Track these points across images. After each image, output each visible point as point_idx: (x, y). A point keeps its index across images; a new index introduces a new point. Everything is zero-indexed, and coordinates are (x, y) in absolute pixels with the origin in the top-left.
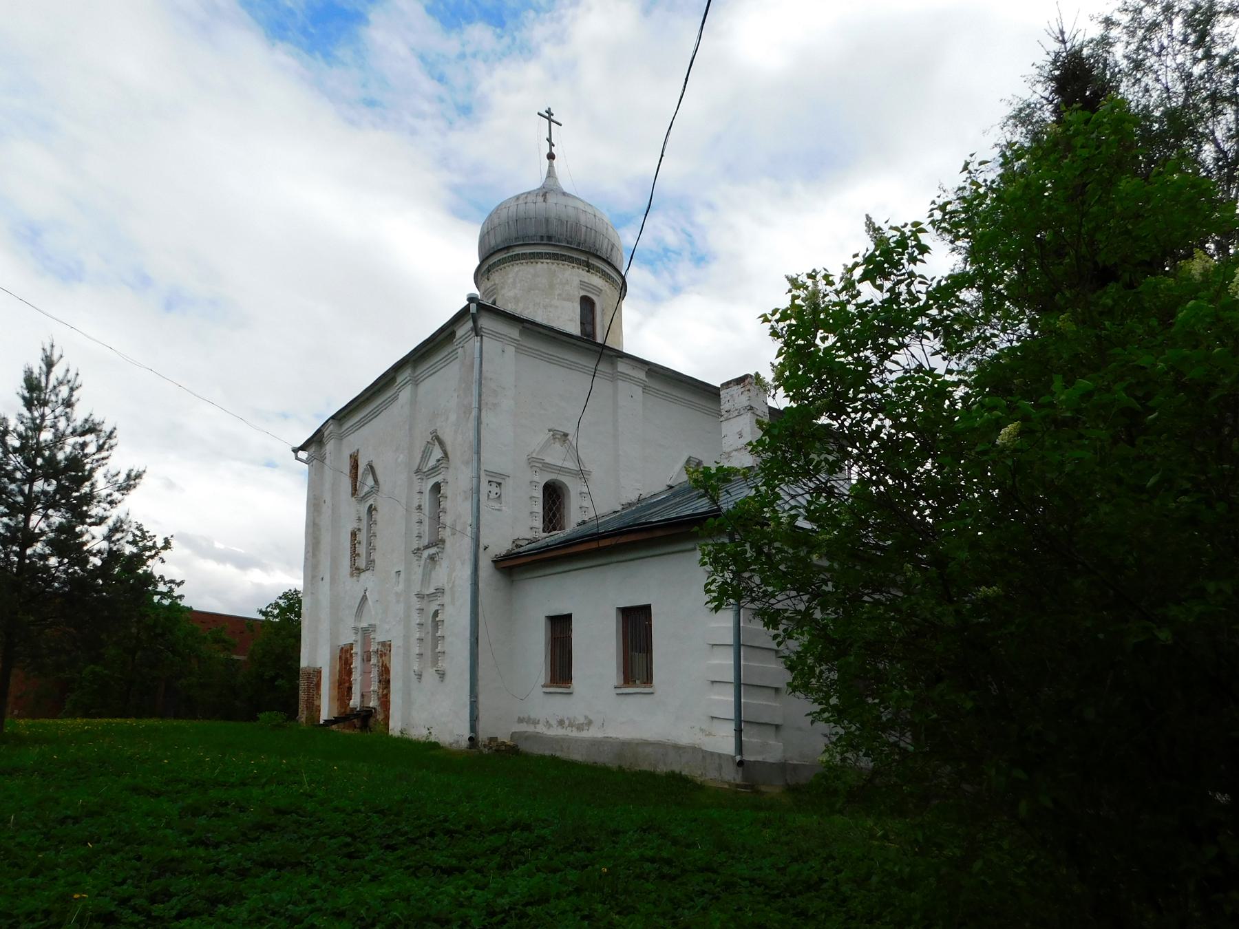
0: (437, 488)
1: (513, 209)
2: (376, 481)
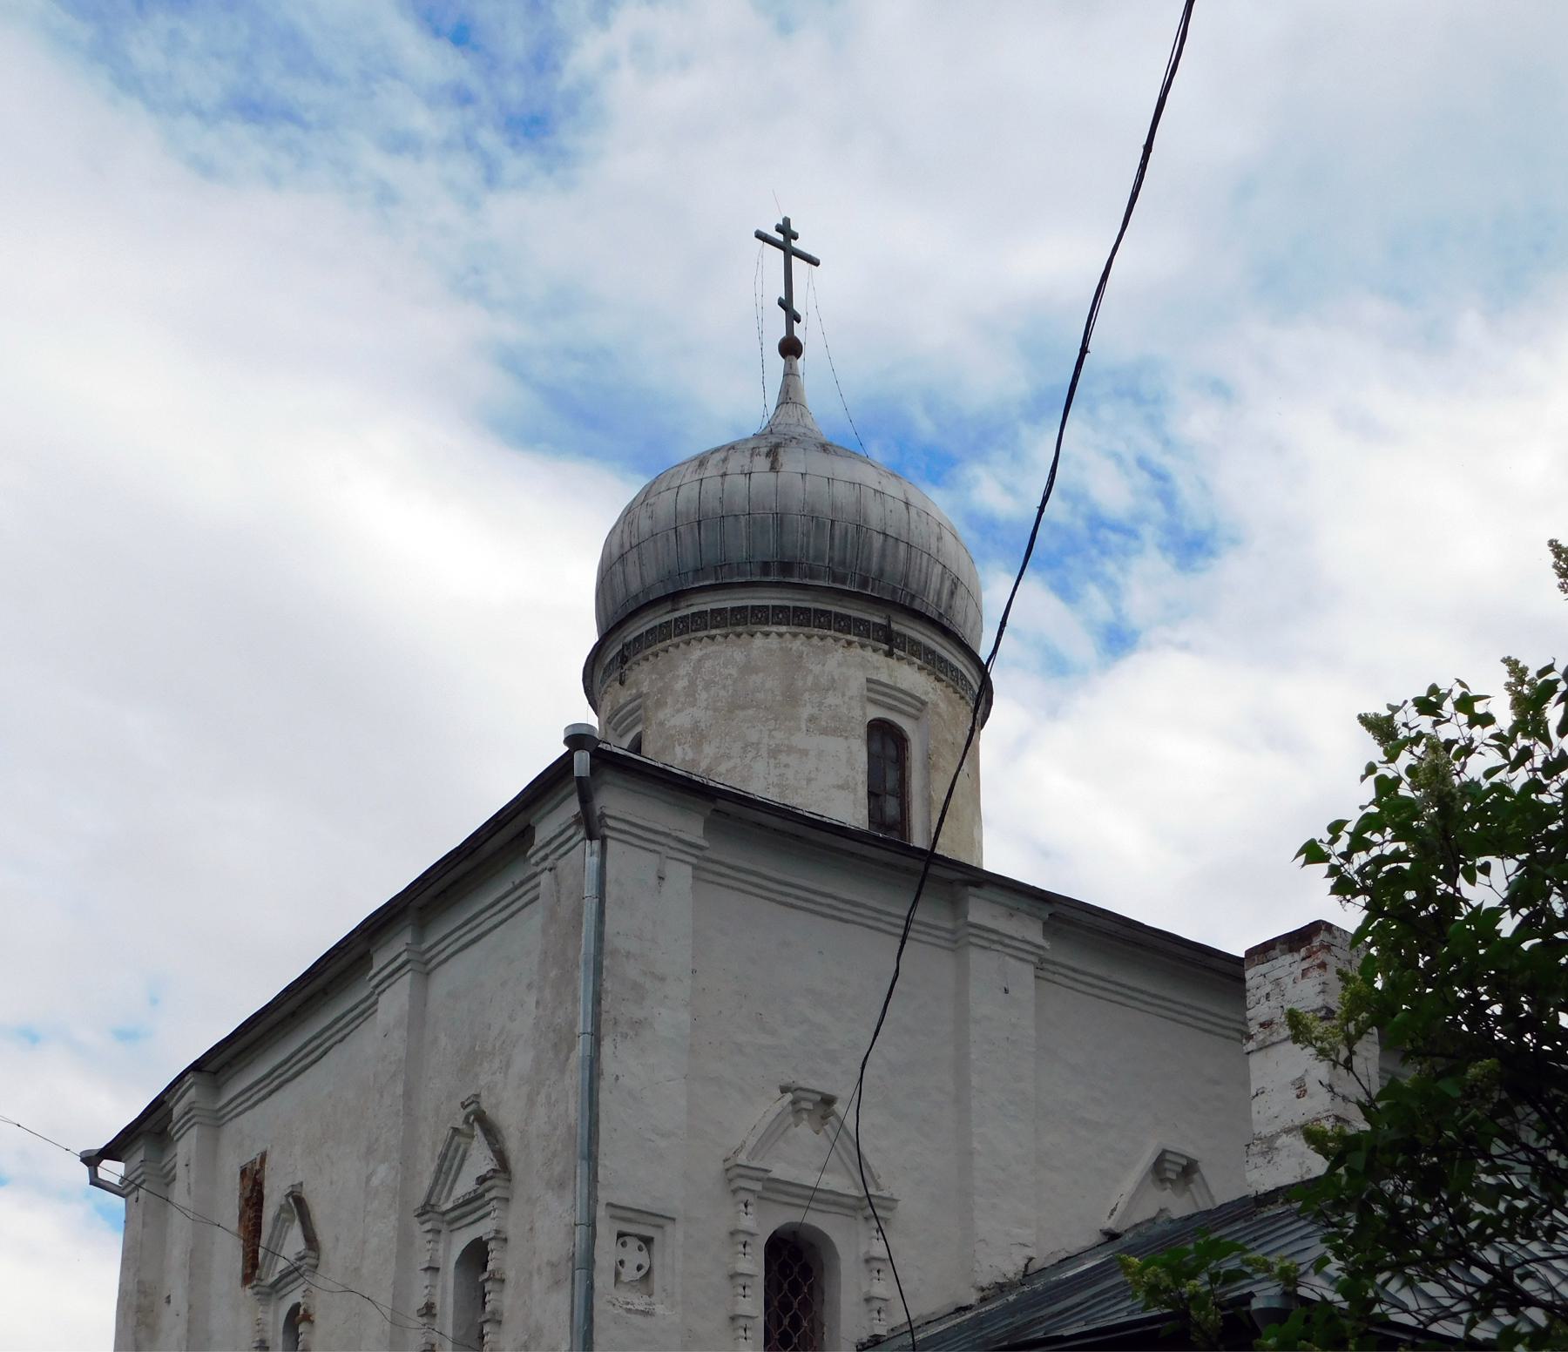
0: (477, 1254)
2: (311, 1240)
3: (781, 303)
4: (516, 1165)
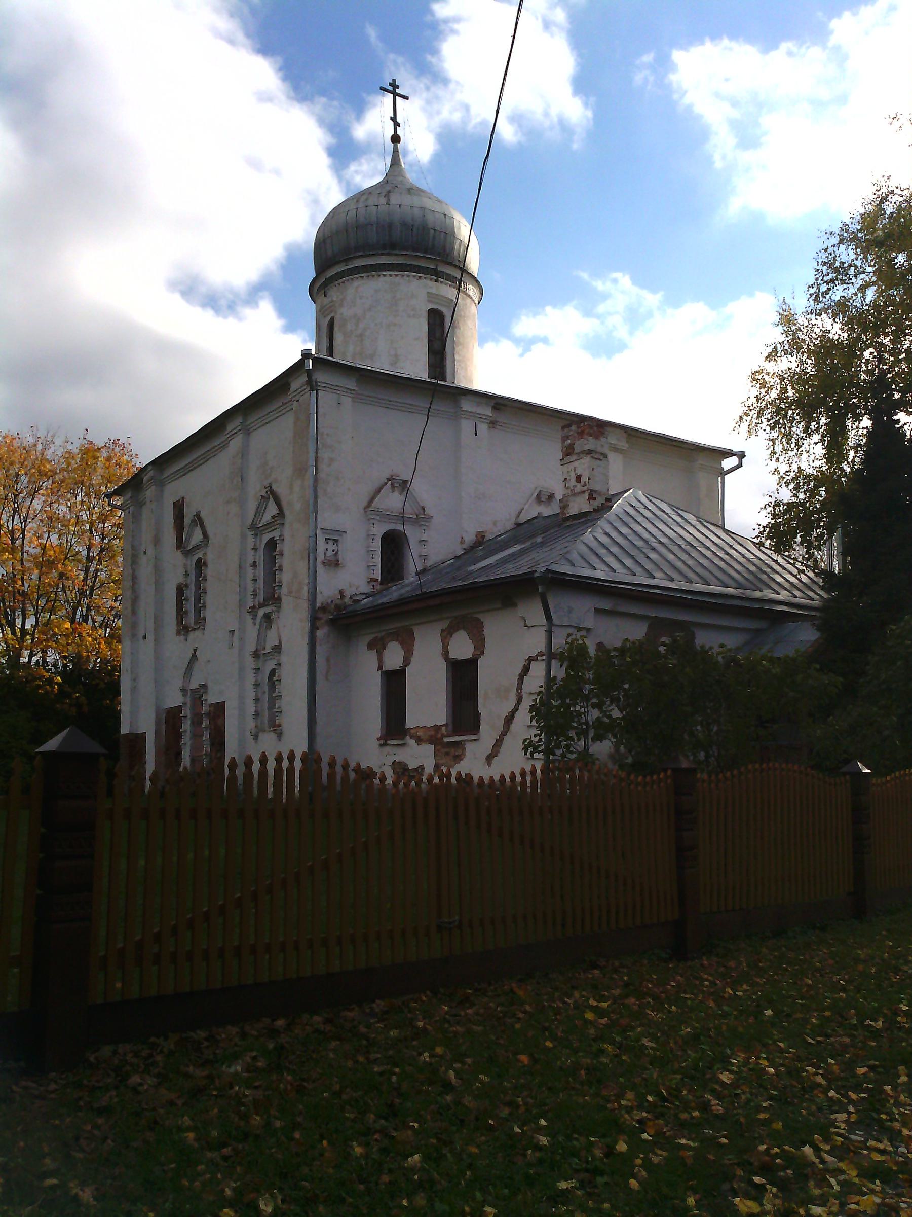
0: (272, 545)
1: (352, 214)
2: (205, 535)
3: (391, 118)
4: (287, 512)
